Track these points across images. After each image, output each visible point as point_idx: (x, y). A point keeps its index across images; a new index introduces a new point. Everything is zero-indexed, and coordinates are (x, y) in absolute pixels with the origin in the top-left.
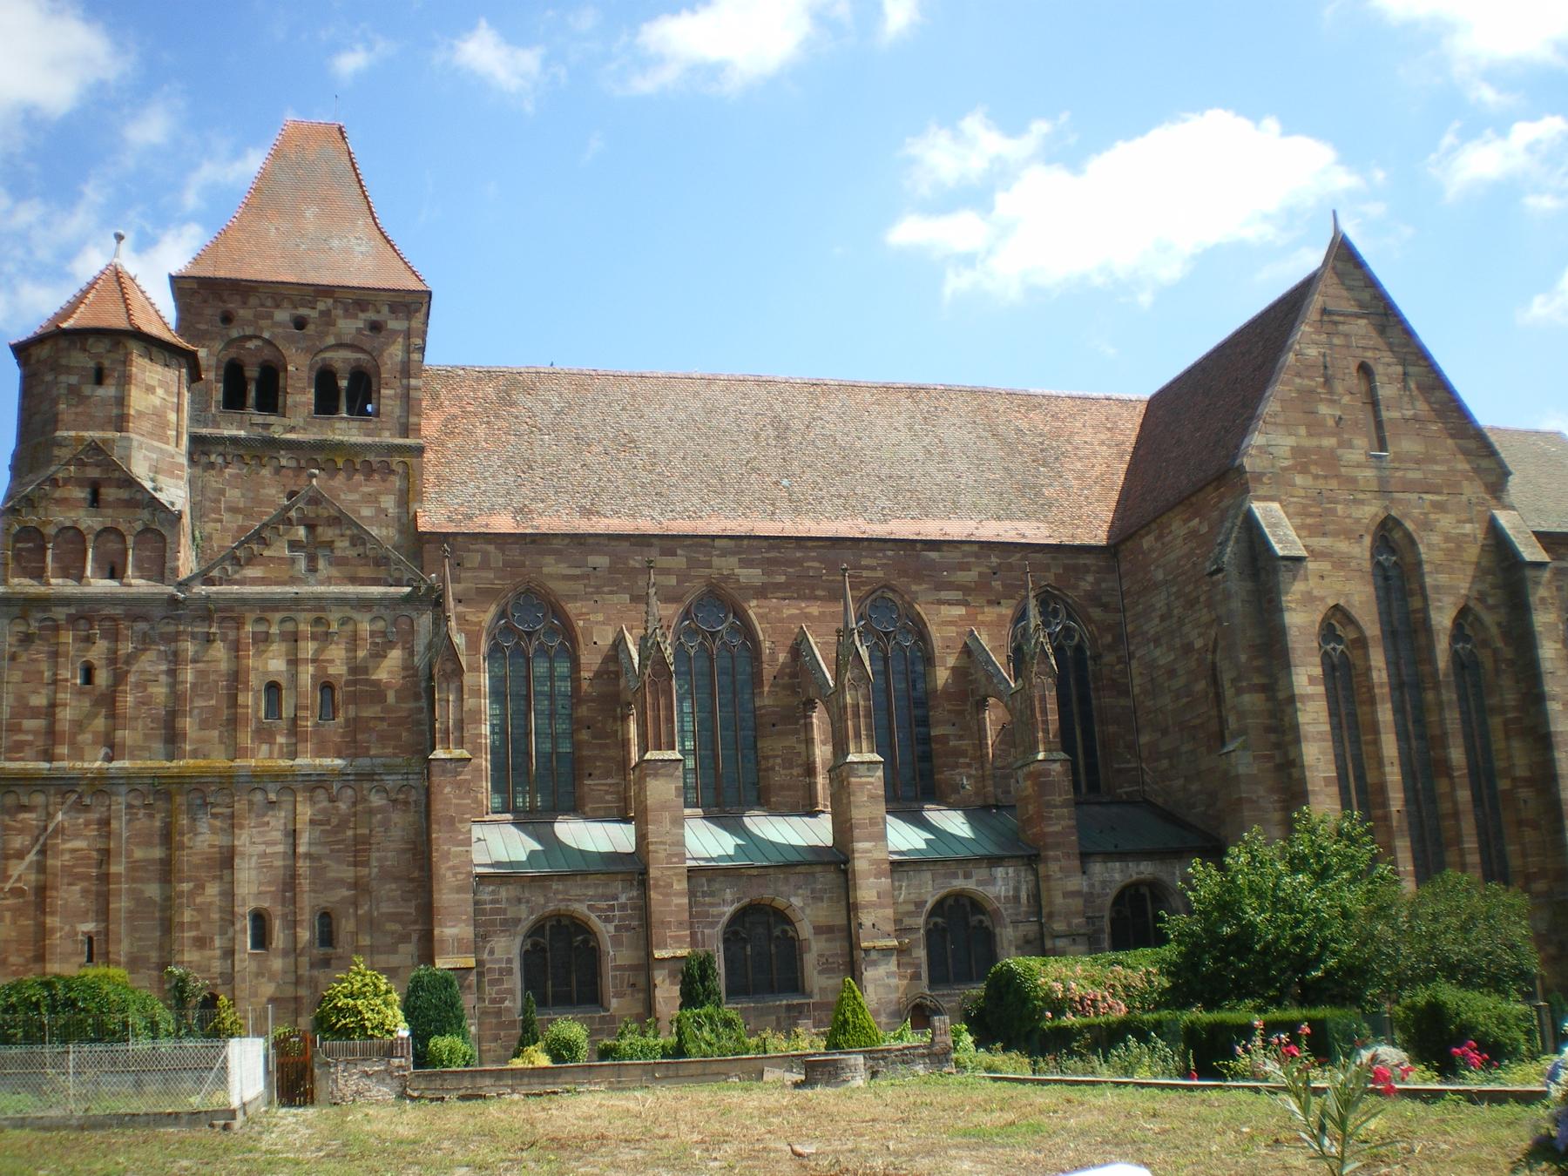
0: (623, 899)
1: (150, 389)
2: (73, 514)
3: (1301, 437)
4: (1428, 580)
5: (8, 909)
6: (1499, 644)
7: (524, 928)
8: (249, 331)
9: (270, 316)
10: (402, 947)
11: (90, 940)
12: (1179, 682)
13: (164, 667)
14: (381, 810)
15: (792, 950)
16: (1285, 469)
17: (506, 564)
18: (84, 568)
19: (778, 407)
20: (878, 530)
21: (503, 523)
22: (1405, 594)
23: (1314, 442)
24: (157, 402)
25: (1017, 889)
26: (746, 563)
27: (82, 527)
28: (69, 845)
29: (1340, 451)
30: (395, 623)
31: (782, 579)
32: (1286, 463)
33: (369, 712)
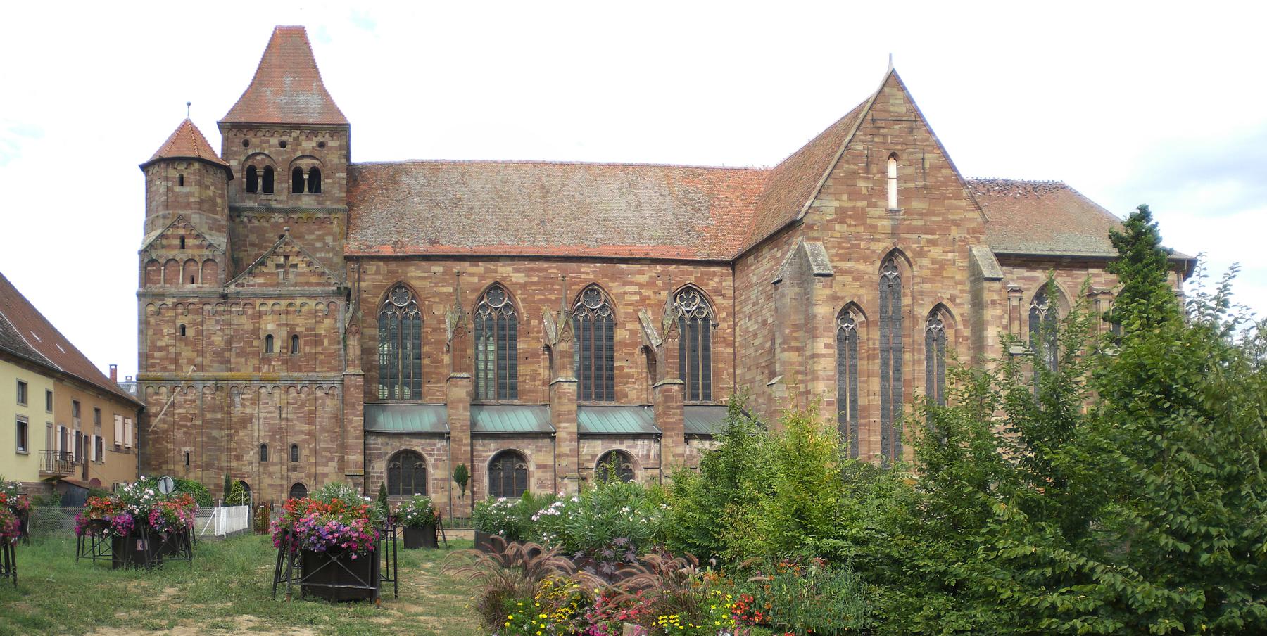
3: (845, 201)
6: (960, 327)
9: (268, 142)
12: (757, 342)
14: (321, 398)
19: (544, 178)
25: (649, 451)
31: (536, 279)
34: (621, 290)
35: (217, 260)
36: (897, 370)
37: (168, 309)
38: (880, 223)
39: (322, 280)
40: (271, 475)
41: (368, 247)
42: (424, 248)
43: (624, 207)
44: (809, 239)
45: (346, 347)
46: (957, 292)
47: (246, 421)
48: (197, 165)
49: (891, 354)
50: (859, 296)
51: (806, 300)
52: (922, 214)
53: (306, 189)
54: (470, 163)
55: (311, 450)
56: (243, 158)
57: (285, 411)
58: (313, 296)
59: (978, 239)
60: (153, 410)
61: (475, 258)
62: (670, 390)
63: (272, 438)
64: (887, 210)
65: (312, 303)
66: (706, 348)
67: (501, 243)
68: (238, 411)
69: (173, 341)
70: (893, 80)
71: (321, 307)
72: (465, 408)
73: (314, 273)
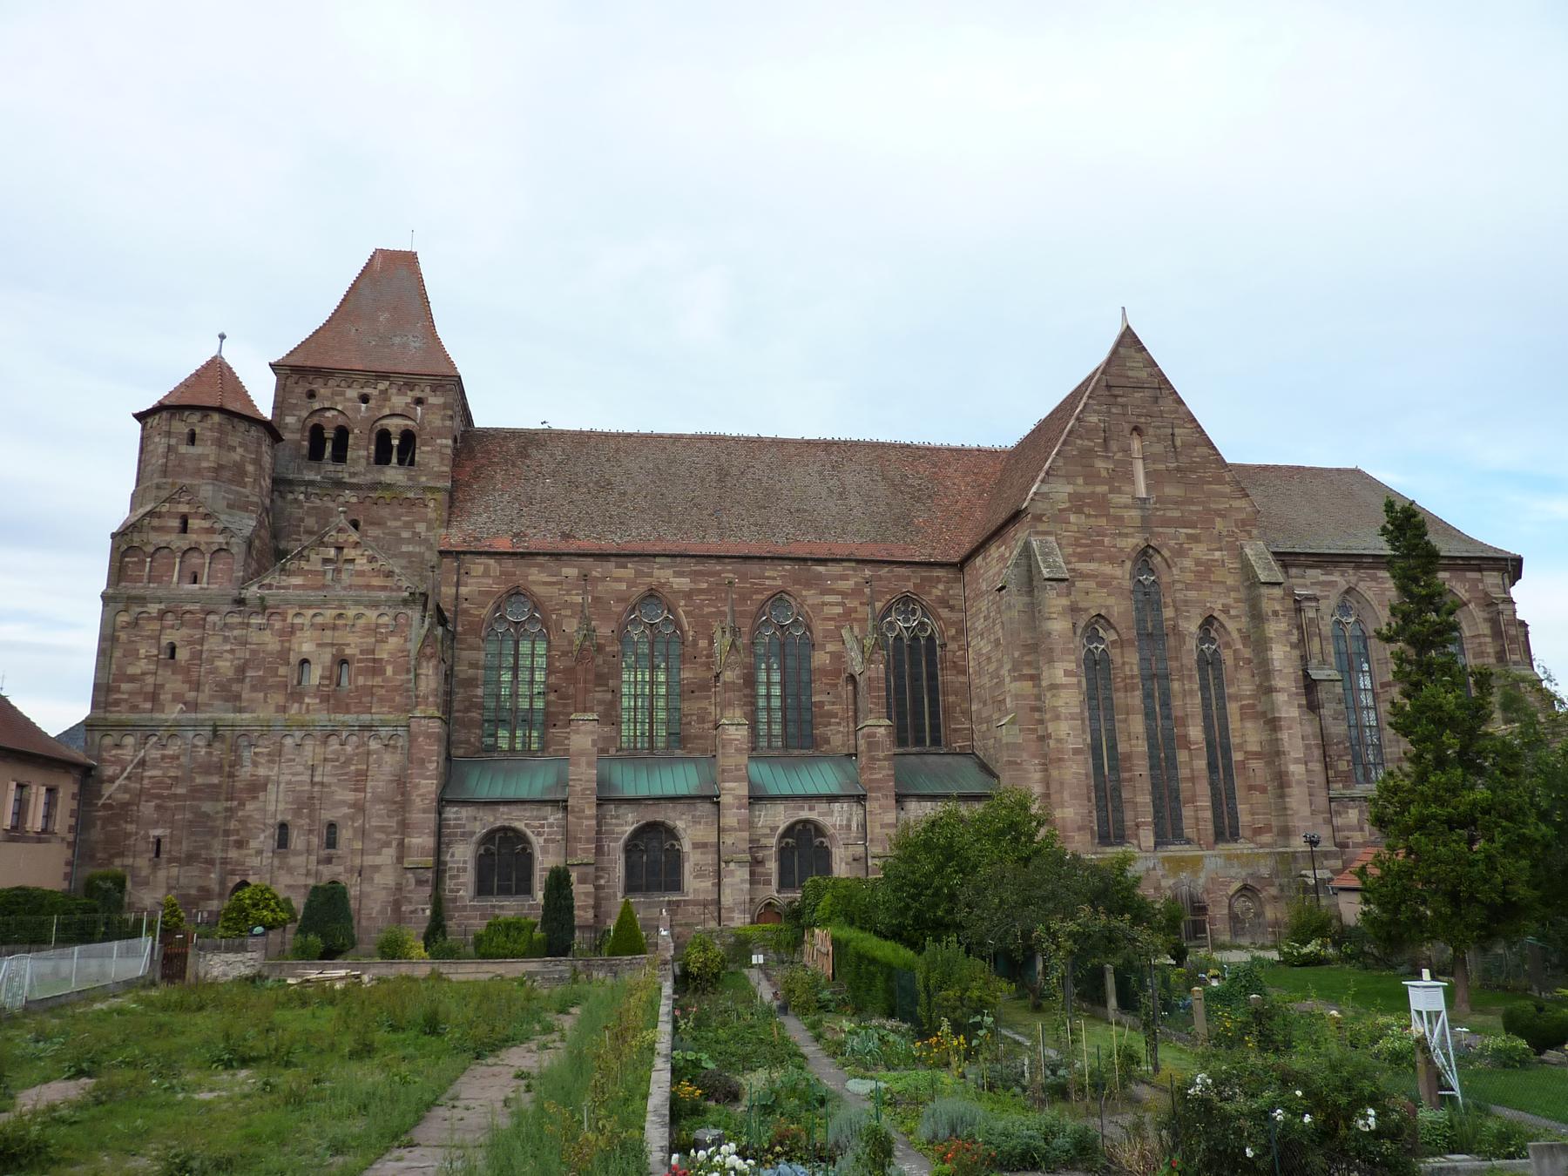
0: (551, 820)
2: (168, 538)
3: (1080, 485)
6: (1239, 646)
9: (343, 394)
10: (385, 851)
14: (376, 752)
15: (676, 859)
19: (723, 458)
23: (1089, 489)
24: (238, 458)
25: (849, 820)
31: (705, 586)
32: (1064, 506)
34: (818, 600)
35: (234, 550)
36: (1166, 704)
37: (151, 619)
38: (1126, 514)
39: (389, 583)
40: (290, 870)
41: (477, 539)
42: (551, 542)
44: (1037, 533)
45: (417, 676)
46: (1230, 601)
47: (257, 787)
48: (216, 417)
49: (1156, 681)
50: (1107, 607)
51: (1034, 613)
52: (1177, 503)
53: (394, 460)
55: (355, 829)
56: (305, 414)
57: (320, 770)
58: (375, 605)
59: (1249, 533)
60: (110, 771)
61: (622, 557)
62: (873, 735)
63: (297, 813)
64: (1134, 498)
65: (372, 614)
66: (932, 677)
67: (659, 538)
68: (245, 772)
69: (153, 667)
70: (1128, 341)
71: (385, 619)
73: (376, 572)
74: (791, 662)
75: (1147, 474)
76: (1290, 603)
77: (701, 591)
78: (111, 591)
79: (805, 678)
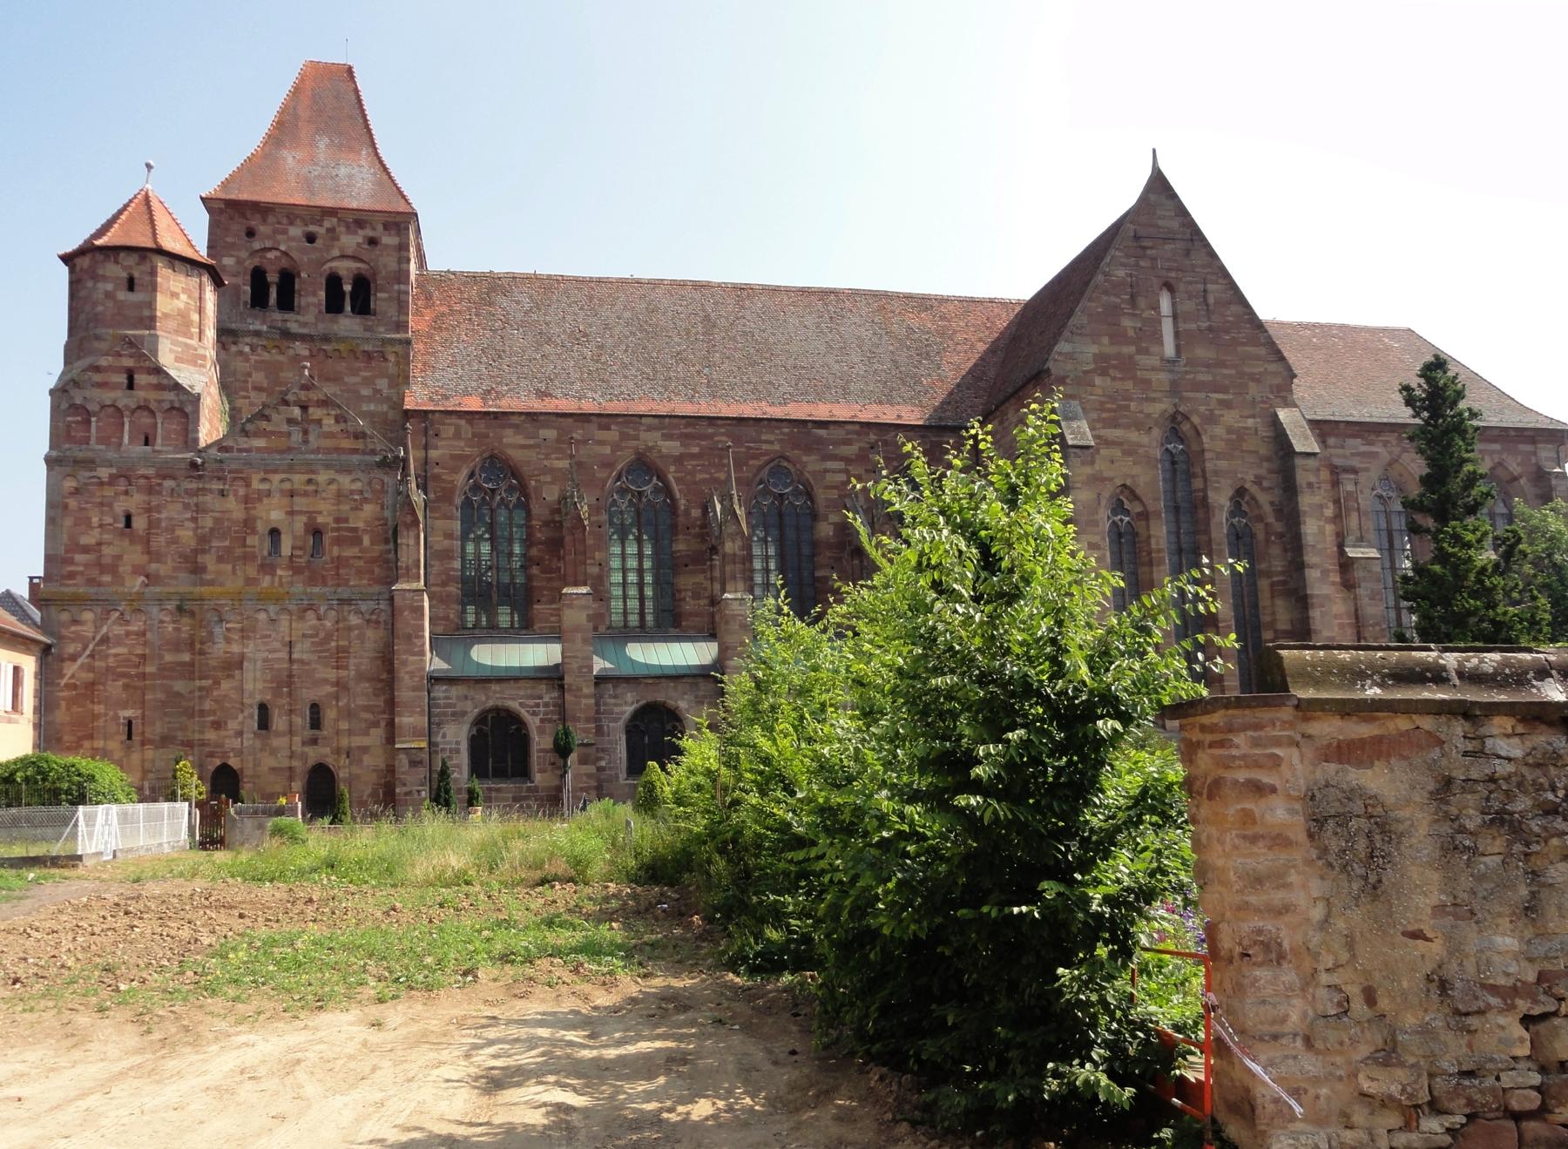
0: (546, 699)
1: (174, 295)
3: (1105, 346)
4: (1209, 466)
5: (64, 699)
6: (1271, 519)
7: (470, 717)
8: (268, 244)
9: (285, 232)
10: (372, 731)
11: (130, 723)
13: (188, 515)
14: (357, 627)
16: (1086, 372)
17: (474, 435)
18: (122, 437)
20: (777, 412)
21: (474, 404)
22: (1189, 476)
24: (182, 306)
26: (667, 437)
27: (120, 405)
28: (113, 651)
29: (1138, 357)
30: (370, 483)
31: (696, 450)
33: (350, 552)
34: (819, 467)
39: (359, 445)
40: (274, 752)
41: (446, 397)
43: (823, 349)
47: (234, 665)
53: (348, 308)
54: (600, 281)
55: (339, 709)
57: (297, 648)
58: (345, 469)
63: (277, 691)
64: (1162, 359)
65: (345, 481)
68: (219, 649)
70: (1159, 186)
72: (585, 641)
74: (790, 534)
75: (1177, 334)
76: (1325, 475)
77: (693, 456)
78: (54, 453)
79: (806, 550)
